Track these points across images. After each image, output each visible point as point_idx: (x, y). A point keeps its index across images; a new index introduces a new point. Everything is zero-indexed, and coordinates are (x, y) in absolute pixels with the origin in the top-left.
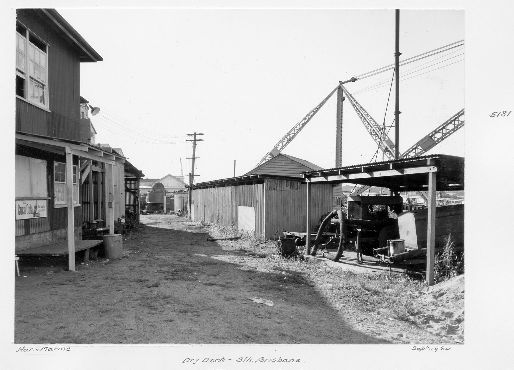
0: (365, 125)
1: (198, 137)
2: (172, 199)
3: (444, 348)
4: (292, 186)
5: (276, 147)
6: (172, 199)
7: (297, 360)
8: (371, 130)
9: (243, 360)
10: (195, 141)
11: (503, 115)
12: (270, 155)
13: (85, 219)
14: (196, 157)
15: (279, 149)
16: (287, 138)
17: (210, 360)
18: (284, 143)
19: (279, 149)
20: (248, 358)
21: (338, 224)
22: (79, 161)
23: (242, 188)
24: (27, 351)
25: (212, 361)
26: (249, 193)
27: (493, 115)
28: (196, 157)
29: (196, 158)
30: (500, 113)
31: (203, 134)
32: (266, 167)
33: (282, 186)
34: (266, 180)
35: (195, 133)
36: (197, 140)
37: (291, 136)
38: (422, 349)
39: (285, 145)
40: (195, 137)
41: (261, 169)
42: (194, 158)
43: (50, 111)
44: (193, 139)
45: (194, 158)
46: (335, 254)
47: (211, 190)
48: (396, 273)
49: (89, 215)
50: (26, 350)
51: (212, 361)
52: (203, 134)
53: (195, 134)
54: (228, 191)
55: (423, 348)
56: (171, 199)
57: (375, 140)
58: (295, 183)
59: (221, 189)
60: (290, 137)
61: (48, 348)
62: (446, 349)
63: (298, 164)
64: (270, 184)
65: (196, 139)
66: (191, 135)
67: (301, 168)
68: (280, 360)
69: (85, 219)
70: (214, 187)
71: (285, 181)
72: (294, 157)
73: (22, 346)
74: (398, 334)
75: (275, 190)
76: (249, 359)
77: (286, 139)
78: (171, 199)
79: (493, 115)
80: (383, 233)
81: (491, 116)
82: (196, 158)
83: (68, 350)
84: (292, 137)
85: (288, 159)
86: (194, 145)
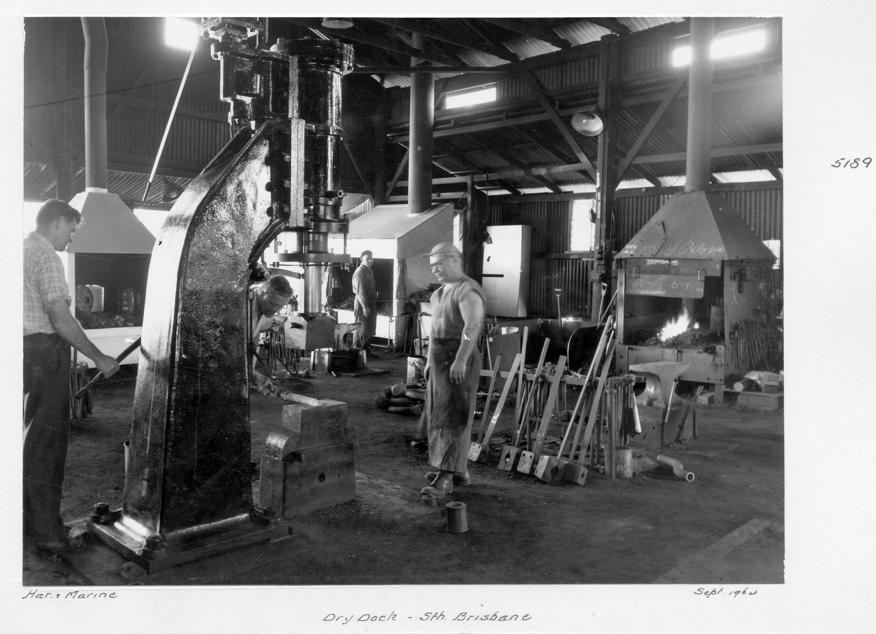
3: (748, 592)
7: (524, 617)
9: (431, 616)
11: (853, 166)
13: (768, 197)
17: (378, 618)
20: (438, 615)
24: (504, 620)
25: (374, 619)
27: (837, 164)
30: (848, 162)
38: (712, 593)
49: (635, 209)
51: (374, 619)
55: (713, 591)
61: (78, 594)
62: (750, 594)
68: (495, 617)
69: (768, 197)
73: (33, 589)
74: (155, 561)
76: (441, 615)
79: (837, 164)
81: (834, 166)
83: (524, 618)
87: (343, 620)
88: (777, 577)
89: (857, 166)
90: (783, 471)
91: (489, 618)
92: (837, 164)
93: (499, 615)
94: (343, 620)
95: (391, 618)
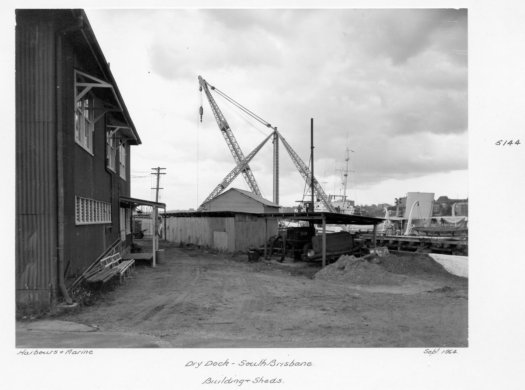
0: (295, 164)
1: (161, 171)
2: (140, 223)
4: (252, 218)
5: (226, 180)
6: (140, 223)
8: (300, 168)
10: (159, 174)
12: (221, 187)
14: (159, 187)
15: (228, 182)
16: (234, 172)
18: (232, 177)
19: (228, 182)
20: (263, 362)
21: (282, 242)
22: (76, 196)
23: (217, 219)
24: (27, 354)
26: (222, 223)
27: (499, 143)
28: (159, 187)
29: (160, 189)
31: (166, 169)
32: (221, 198)
33: (246, 219)
34: (236, 215)
35: (159, 168)
36: (160, 174)
37: (238, 171)
39: (233, 179)
40: (159, 171)
41: (217, 199)
42: (158, 189)
43: (126, 181)
44: (157, 172)
45: (158, 189)
46: (280, 258)
47: (188, 219)
48: (364, 333)
50: (27, 353)
52: (166, 169)
53: (159, 169)
54: (204, 221)
56: (139, 223)
57: (303, 177)
58: (254, 217)
59: (197, 219)
60: (237, 172)
61: (72, 352)
63: (246, 196)
64: (239, 218)
65: (160, 173)
66: (155, 169)
67: (249, 199)
68: (292, 364)
70: (190, 217)
71: (248, 216)
72: (242, 190)
73: (23, 350)
75: (241, 221)
77: (233, 173)
78: (139, 223)
80: (305, 247)
82: (160, 189)
84: (238, 172)
85: (238, 192)
86: (158, 178)
87: (196, 365)
88: (465, 344)
89: (499, 145)
90: (468, 294)
91: (289, 364)
92: (499, 143)
93: (295, 362)
94: (196, 365)
95: (225, 364)
